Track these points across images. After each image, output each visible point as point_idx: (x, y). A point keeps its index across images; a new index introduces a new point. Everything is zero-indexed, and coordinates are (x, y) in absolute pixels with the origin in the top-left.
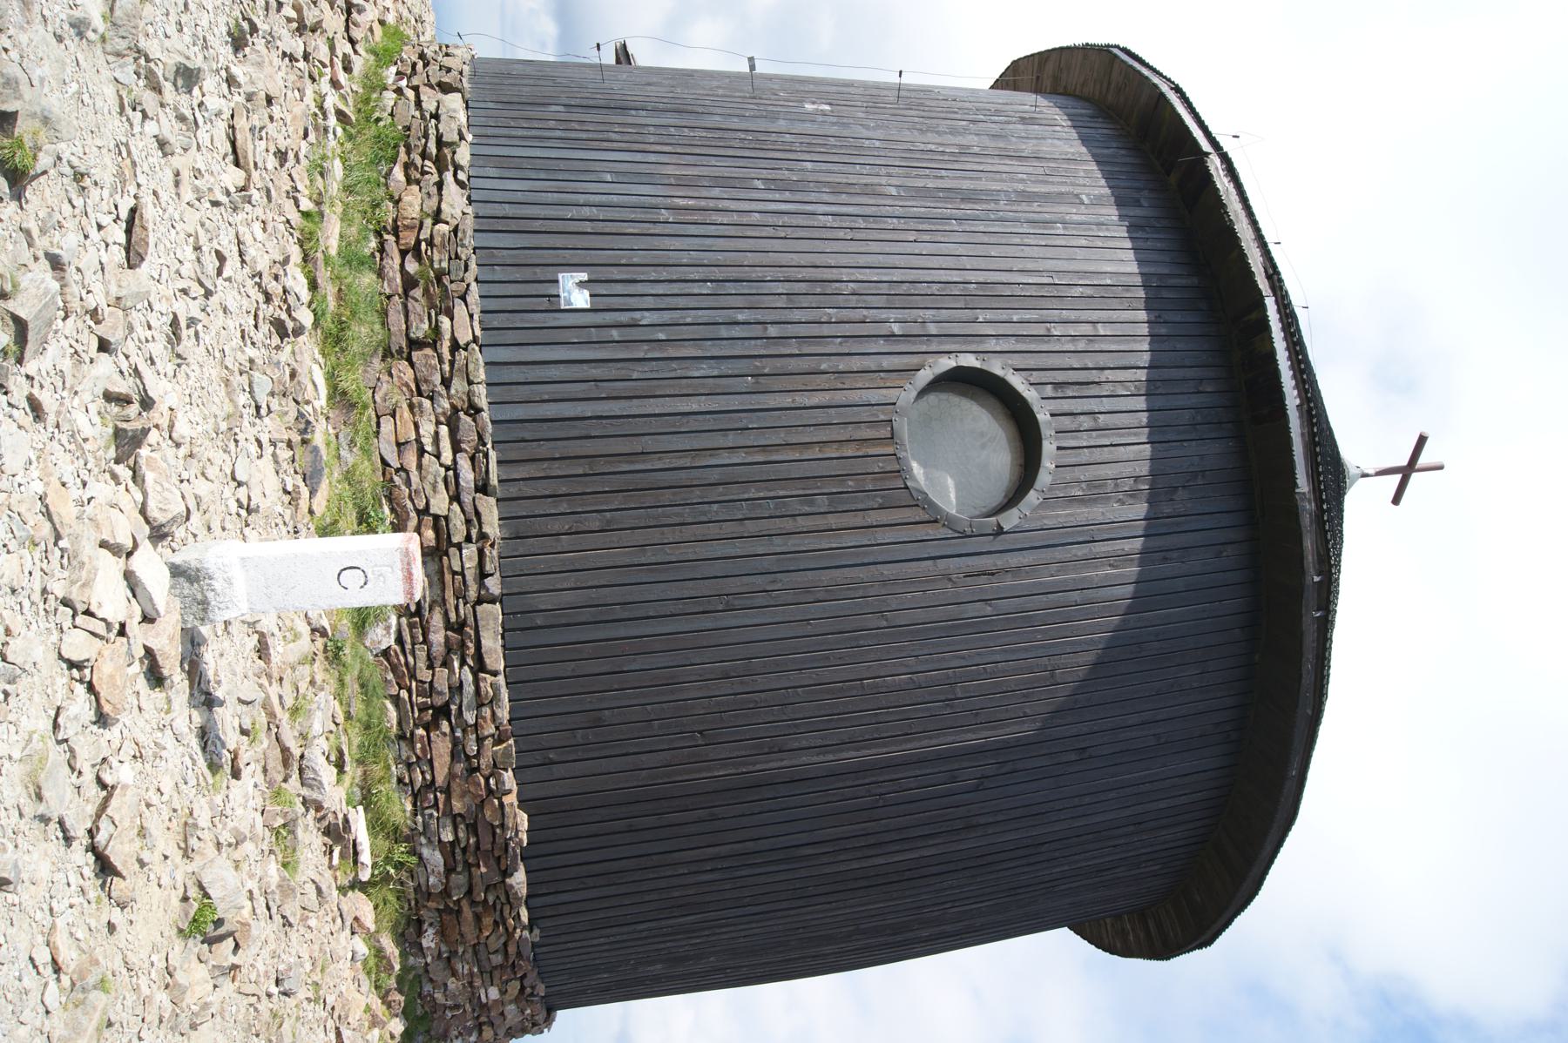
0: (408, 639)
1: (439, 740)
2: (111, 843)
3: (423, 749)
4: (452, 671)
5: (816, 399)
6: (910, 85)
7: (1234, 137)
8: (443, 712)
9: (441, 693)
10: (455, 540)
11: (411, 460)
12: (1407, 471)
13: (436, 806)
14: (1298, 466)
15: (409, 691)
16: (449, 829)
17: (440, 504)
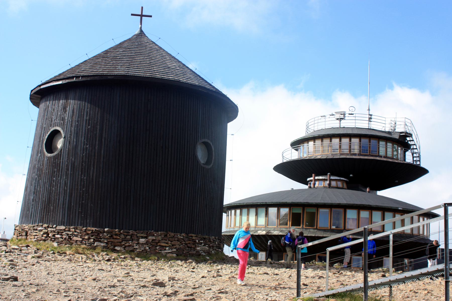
0: (58, 241)
1: (73, 238)
2: (142, 277)
3: (74, 241)
4: (64, 235)
5: (188, 196)
6: (234, 203)
7: (231, 160)
8: (70, 237)
9: (66, 237)
10: (47, 231)
11: (36, 237)
12: (142, 16)
13: (86, 241)
14: (349, 245)
15: (65, 242)
16: (91, 240)
17: (42, 233)
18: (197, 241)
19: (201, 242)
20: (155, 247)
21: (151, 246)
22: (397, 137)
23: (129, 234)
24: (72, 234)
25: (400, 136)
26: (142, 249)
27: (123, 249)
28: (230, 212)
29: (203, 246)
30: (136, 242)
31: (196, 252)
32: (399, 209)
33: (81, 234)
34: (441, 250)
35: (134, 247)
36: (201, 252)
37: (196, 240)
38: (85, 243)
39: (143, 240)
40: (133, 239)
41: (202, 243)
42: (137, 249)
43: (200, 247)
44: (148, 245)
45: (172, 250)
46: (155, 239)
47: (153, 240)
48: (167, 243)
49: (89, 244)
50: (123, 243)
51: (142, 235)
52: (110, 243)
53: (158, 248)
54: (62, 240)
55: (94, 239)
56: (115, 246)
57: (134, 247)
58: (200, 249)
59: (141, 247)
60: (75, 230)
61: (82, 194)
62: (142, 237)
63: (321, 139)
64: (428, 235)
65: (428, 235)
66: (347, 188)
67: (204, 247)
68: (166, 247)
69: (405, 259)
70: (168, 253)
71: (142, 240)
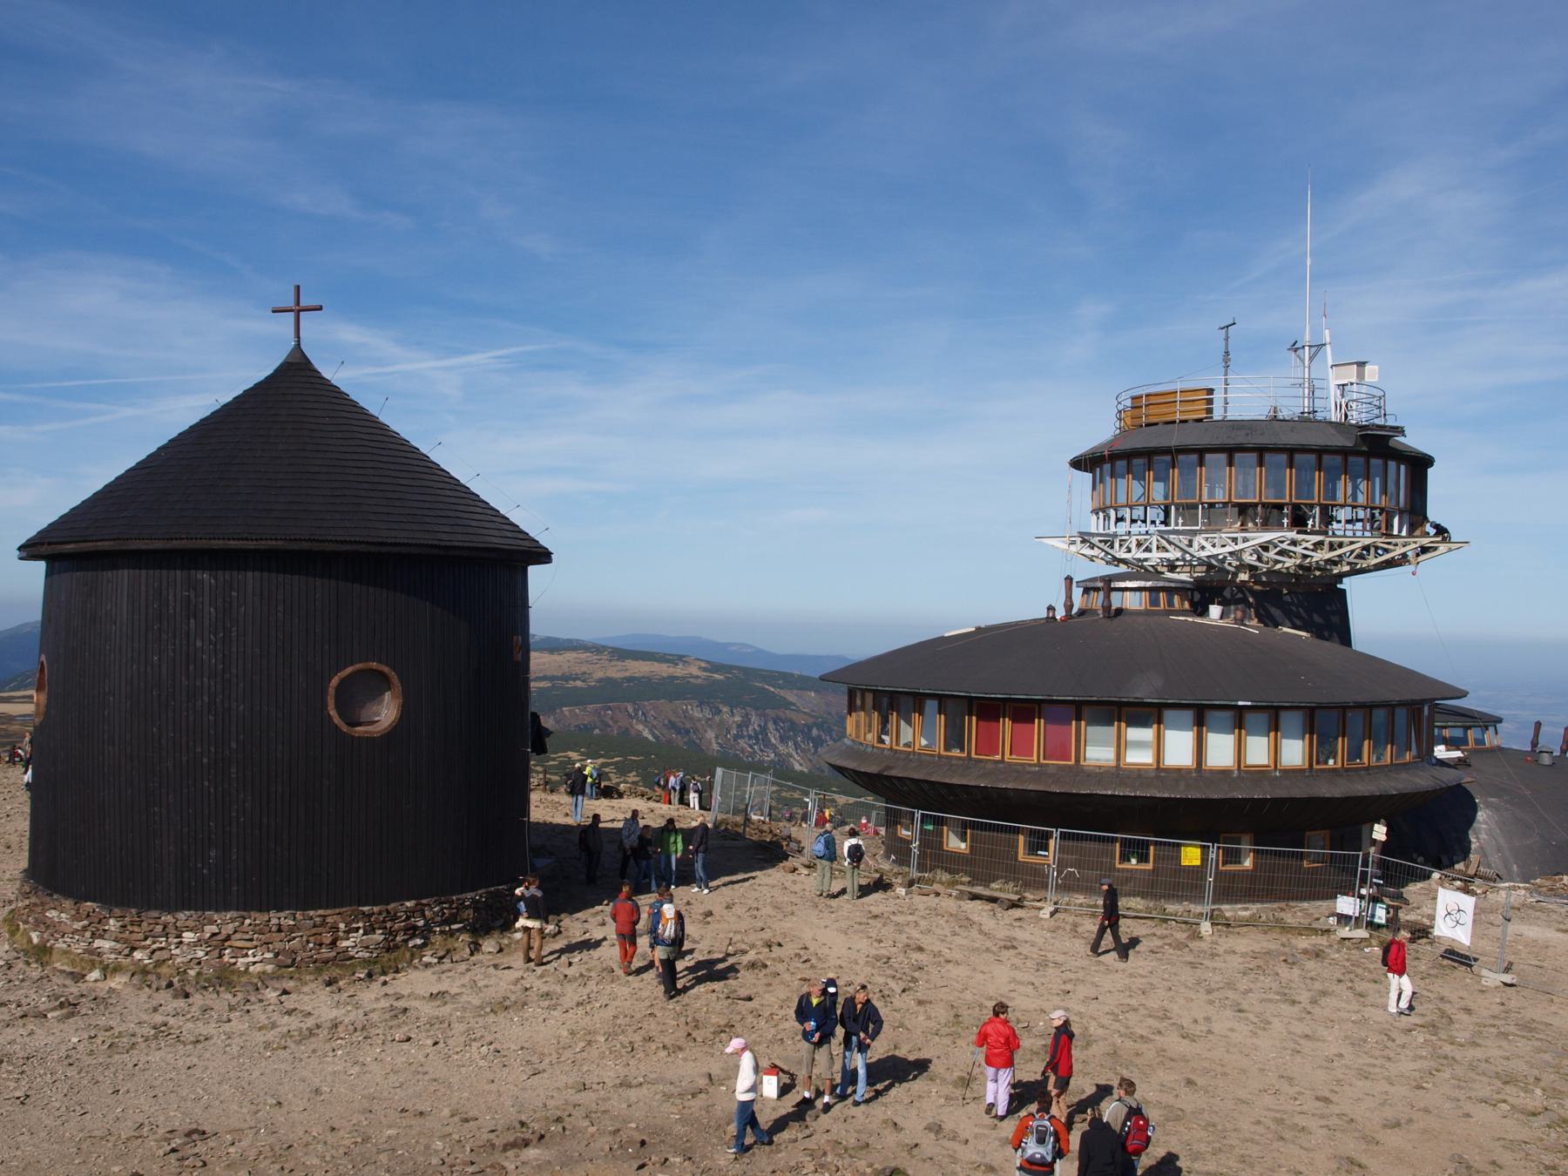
18: (342, 926)
41: (358, 928)
64: (681, 975)
65: (681, 975)
71: (188, 936)
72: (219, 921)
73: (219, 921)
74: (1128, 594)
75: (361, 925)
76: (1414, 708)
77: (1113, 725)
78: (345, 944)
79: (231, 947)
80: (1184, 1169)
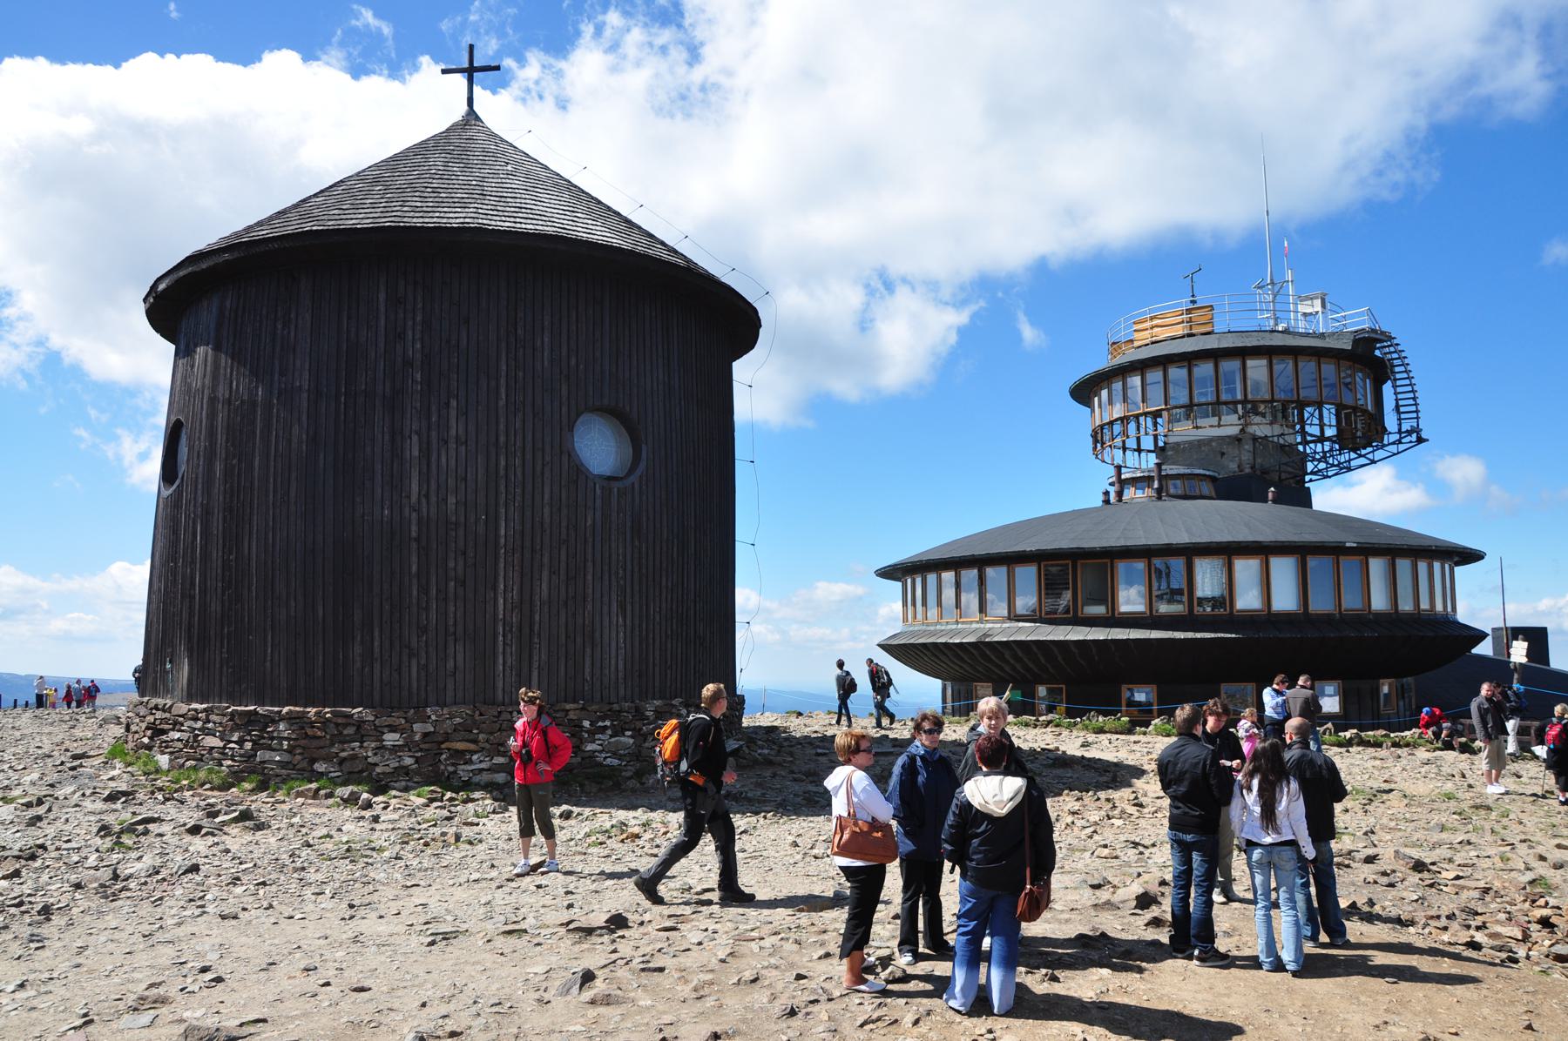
18: (586, 724)
19: (600, 724)
20: (436, 754)
21: (419, 754)
22: (1347, 345)
23: (350, 721)
24: (202, 729)
25: (1356, 342)
26: (392, 766)
27: (332, 769)
28: (909, 581)
29: (611, 736)
30: (373, 745)
31: (583, 759)
32: (1348, 545)
33: (221, 729)
34: (1509, 632)
35: (369, 760)
36: (604, 755)
37: (580, 720)
38: (233, 755)
39: (396, 736)
40: (363, 736)
41: (605, 728)
42: (376, 765)
43: (600, 742)
44: (410, 750)
45: (491, 760)
46: (432, 729)
47: (426, 735)
48: (475, 741)
49: (241, 756)
50: (334, 750)
51: (389, 721)
52: (298, 751)
53: (446, 760)
54: (182, 746)
55: (255, 743)
56: (313, 761)
57: (369, 760)
58: (600, 748)
59: (387, 760)
60: (207, 716)
61: (227, 604)
62: (393, 729)
63: (1139, 372)
64: (1449, 609)
65: (1449, 609)
66: (1213, 494)
67: (613, 740)
68: (473, 752)
69: (1381, 681)
70: (477, 772)
71: (391, 738)
72: (433, 717)
73: (433, 717)
74: (1187, 392)
75: (608, 723)
76: (88, 690)
77: (1309, 488)
78: (590, 747)
79: (449, 749)
80: (562, 65)
